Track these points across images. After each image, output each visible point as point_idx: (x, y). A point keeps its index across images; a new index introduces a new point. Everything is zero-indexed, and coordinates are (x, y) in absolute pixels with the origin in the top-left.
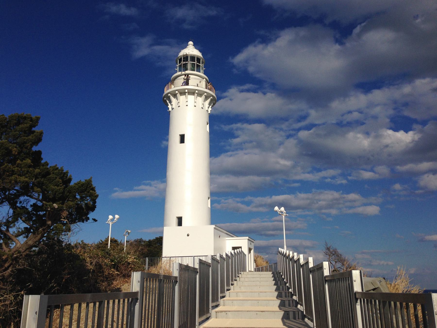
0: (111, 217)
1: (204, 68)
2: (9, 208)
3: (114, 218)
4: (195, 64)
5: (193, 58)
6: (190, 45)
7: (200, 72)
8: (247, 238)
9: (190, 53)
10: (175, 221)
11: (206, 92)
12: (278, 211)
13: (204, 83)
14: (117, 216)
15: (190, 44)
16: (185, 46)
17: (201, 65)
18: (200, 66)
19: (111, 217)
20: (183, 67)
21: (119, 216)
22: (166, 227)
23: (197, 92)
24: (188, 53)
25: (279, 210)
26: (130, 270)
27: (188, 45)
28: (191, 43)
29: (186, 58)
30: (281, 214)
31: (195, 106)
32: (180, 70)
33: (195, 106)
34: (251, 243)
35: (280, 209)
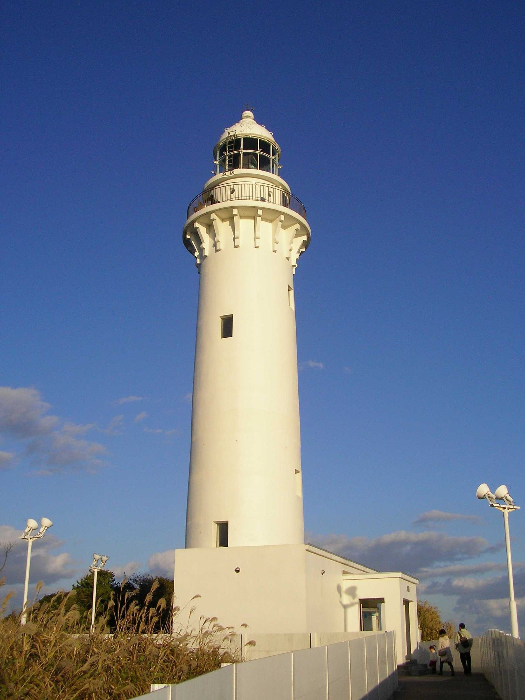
0: (32, 523)
1: (280, 165)
2: (507, 493)
3: (40, 525)
4: (244, 149)
5: (250, 142)
6: (245, 118)
7: (268, 170)
8: (400, 574)
9: (243, 133)
10: (214, 532)
11: (283, 214)
12: (487, 496)
13: (278, 195)
14: (46, 522)
15: (248, 117)
16: (238, 118)
17: (272, 157)
18: (268, 160)
19: (32, 523)
20: (229, 162)
21: (52, 522)
22: (191, 549)
23: (260, 212)
24: (240, 133)
25: (491, 495)
26: (104, 673)
27: (242, 119)
28: (248, 114)
29: (235, 143)
30: (498, 505)
31: (275, 251)
32: (223, 170)
33: (275, 251)
34: (408, 587)
35: (493, 492)
